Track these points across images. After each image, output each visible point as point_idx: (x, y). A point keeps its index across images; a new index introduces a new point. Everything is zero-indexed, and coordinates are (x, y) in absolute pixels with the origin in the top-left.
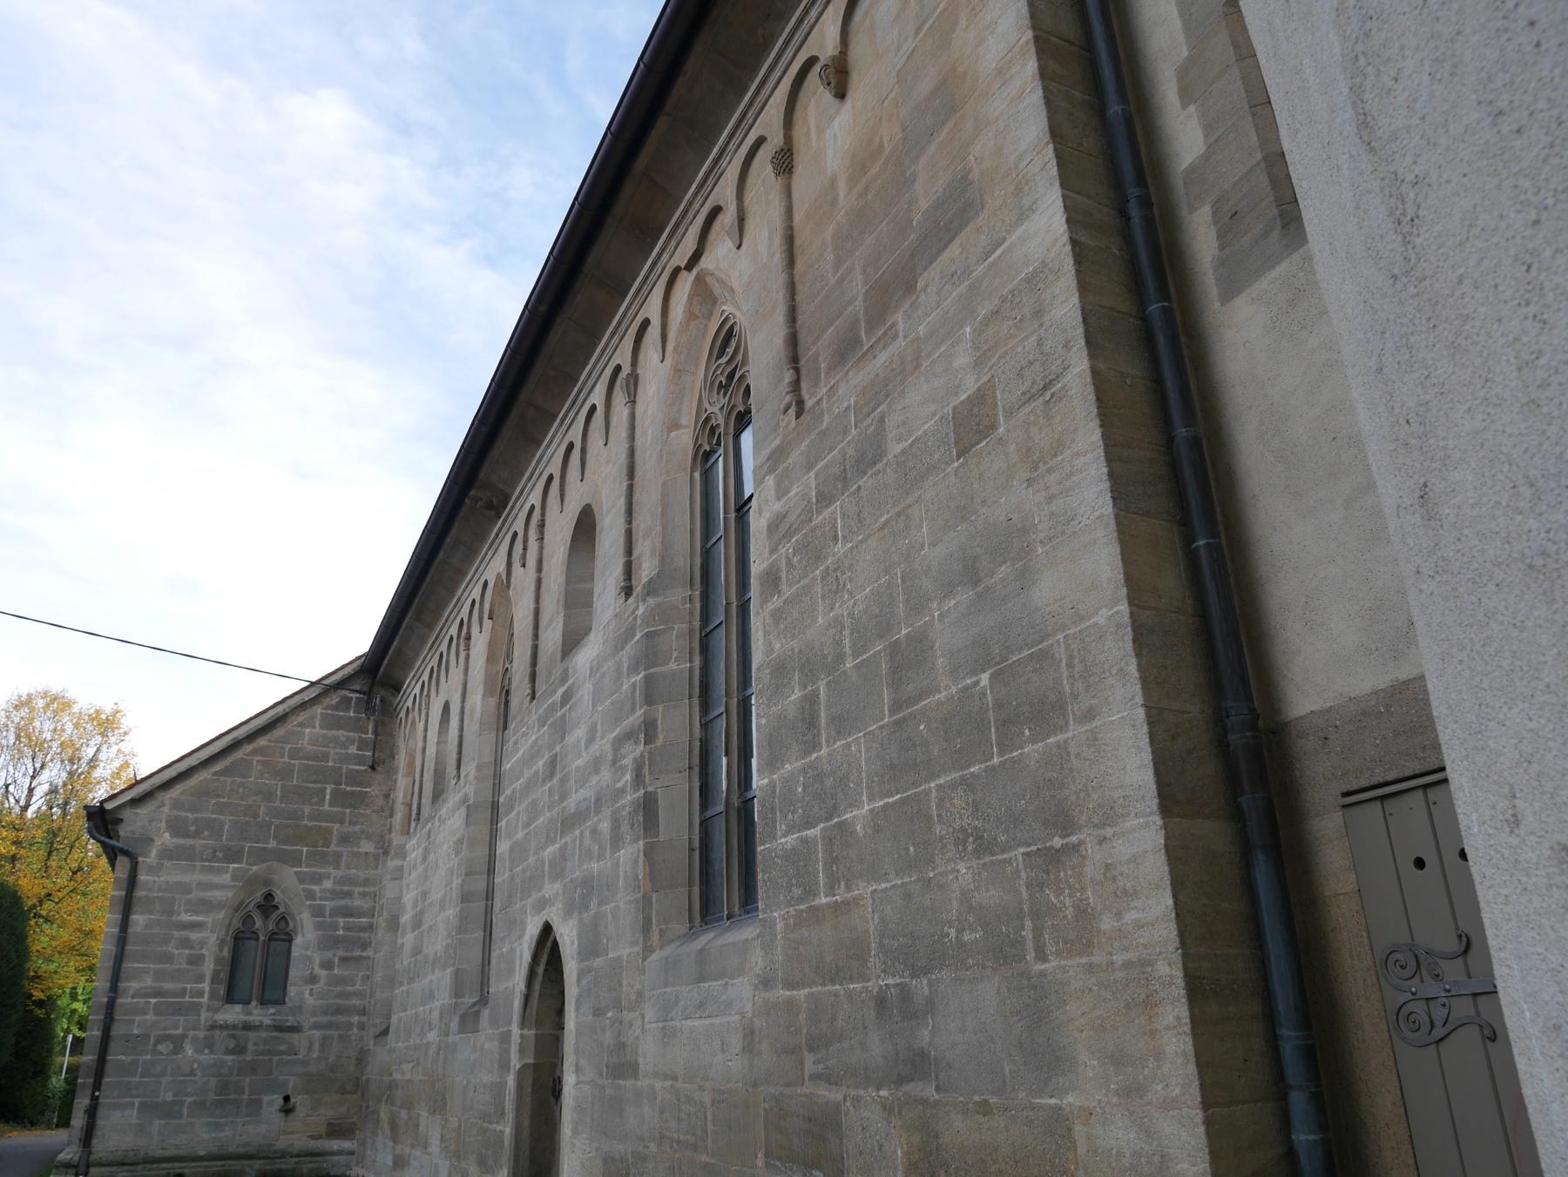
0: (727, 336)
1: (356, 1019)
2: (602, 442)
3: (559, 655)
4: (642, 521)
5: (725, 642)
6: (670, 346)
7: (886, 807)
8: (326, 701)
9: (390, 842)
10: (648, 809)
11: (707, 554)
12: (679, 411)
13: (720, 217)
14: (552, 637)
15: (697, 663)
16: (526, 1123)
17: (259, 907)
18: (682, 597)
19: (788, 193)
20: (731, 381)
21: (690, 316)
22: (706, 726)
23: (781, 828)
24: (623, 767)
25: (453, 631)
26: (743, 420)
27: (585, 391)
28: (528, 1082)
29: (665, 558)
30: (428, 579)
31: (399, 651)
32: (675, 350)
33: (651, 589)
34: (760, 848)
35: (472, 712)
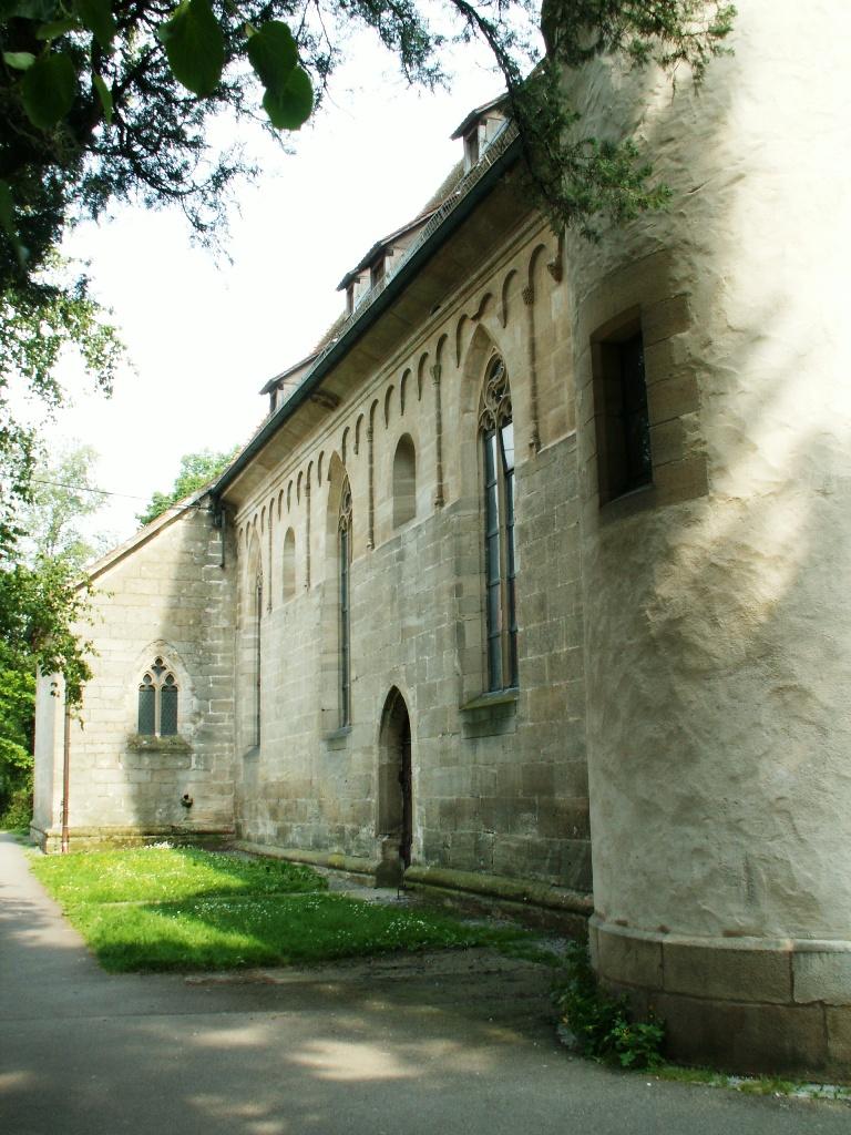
0: (496, 366)
1: (226, 745)
2: (417, 396)
3: (391, 525)
4: (449, 464)
5: (499, 544)
6: (463, 361)
7: (573, 651)
8: (186, 517)
9: (241, 621)
10: (459, 631)
11: (488, 490)
12: (469, 402)
13: (491, 300)
14: (385, 510)
15: (483, 510)
16: (385, 796)
17: (153, 668)
18: (472, 513)
19: (531, 315)
20: (500, 392)
21: (475, 346)
22: (489, 587)
23: (529, 652)
24: (443, 607)
25: (294, 477)
26: (507, 421)
27: (402, 359)
28: (385, 775)
29: (464, 492)
30: (274, 438)
31: (242, 481)
32: (467, 363)
33: (455, 508)
34: (520, 660)
35: (317, 543)
